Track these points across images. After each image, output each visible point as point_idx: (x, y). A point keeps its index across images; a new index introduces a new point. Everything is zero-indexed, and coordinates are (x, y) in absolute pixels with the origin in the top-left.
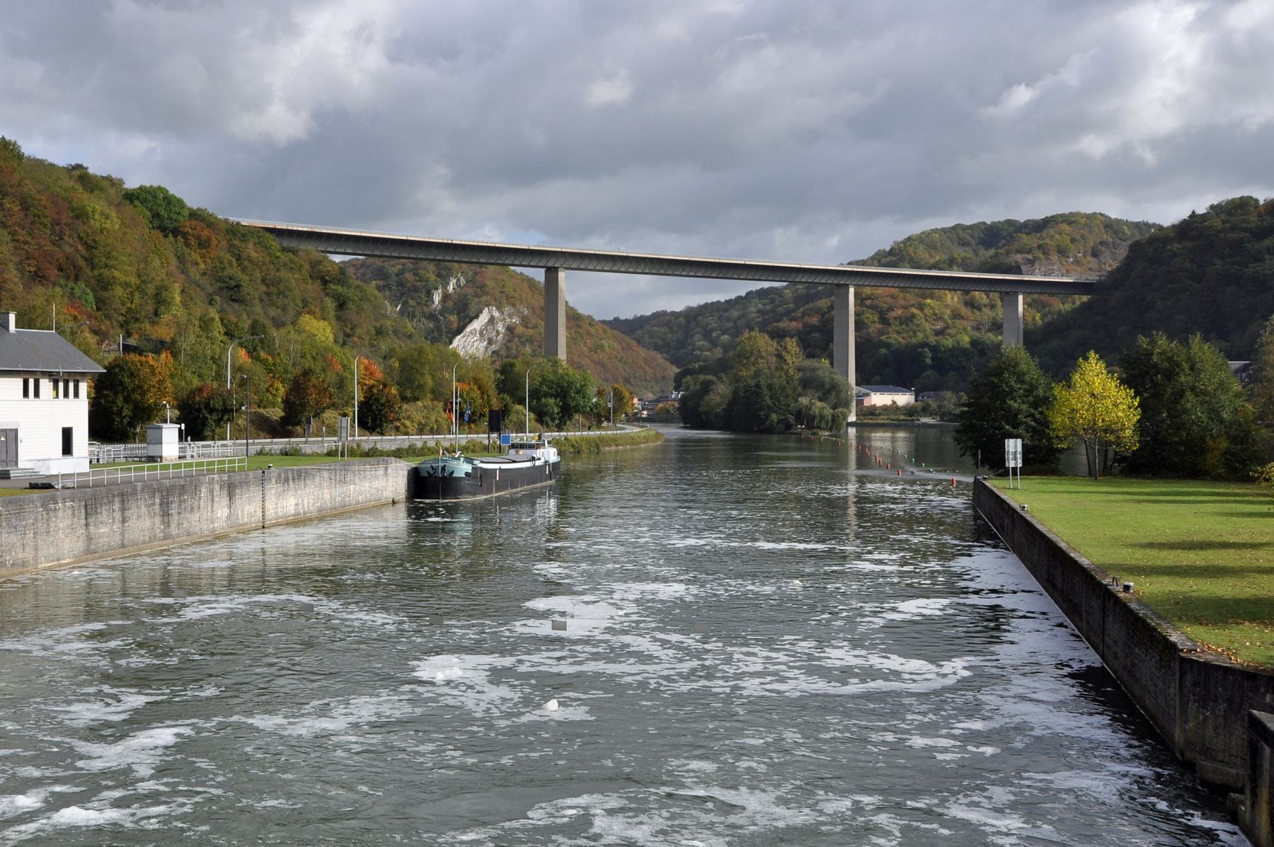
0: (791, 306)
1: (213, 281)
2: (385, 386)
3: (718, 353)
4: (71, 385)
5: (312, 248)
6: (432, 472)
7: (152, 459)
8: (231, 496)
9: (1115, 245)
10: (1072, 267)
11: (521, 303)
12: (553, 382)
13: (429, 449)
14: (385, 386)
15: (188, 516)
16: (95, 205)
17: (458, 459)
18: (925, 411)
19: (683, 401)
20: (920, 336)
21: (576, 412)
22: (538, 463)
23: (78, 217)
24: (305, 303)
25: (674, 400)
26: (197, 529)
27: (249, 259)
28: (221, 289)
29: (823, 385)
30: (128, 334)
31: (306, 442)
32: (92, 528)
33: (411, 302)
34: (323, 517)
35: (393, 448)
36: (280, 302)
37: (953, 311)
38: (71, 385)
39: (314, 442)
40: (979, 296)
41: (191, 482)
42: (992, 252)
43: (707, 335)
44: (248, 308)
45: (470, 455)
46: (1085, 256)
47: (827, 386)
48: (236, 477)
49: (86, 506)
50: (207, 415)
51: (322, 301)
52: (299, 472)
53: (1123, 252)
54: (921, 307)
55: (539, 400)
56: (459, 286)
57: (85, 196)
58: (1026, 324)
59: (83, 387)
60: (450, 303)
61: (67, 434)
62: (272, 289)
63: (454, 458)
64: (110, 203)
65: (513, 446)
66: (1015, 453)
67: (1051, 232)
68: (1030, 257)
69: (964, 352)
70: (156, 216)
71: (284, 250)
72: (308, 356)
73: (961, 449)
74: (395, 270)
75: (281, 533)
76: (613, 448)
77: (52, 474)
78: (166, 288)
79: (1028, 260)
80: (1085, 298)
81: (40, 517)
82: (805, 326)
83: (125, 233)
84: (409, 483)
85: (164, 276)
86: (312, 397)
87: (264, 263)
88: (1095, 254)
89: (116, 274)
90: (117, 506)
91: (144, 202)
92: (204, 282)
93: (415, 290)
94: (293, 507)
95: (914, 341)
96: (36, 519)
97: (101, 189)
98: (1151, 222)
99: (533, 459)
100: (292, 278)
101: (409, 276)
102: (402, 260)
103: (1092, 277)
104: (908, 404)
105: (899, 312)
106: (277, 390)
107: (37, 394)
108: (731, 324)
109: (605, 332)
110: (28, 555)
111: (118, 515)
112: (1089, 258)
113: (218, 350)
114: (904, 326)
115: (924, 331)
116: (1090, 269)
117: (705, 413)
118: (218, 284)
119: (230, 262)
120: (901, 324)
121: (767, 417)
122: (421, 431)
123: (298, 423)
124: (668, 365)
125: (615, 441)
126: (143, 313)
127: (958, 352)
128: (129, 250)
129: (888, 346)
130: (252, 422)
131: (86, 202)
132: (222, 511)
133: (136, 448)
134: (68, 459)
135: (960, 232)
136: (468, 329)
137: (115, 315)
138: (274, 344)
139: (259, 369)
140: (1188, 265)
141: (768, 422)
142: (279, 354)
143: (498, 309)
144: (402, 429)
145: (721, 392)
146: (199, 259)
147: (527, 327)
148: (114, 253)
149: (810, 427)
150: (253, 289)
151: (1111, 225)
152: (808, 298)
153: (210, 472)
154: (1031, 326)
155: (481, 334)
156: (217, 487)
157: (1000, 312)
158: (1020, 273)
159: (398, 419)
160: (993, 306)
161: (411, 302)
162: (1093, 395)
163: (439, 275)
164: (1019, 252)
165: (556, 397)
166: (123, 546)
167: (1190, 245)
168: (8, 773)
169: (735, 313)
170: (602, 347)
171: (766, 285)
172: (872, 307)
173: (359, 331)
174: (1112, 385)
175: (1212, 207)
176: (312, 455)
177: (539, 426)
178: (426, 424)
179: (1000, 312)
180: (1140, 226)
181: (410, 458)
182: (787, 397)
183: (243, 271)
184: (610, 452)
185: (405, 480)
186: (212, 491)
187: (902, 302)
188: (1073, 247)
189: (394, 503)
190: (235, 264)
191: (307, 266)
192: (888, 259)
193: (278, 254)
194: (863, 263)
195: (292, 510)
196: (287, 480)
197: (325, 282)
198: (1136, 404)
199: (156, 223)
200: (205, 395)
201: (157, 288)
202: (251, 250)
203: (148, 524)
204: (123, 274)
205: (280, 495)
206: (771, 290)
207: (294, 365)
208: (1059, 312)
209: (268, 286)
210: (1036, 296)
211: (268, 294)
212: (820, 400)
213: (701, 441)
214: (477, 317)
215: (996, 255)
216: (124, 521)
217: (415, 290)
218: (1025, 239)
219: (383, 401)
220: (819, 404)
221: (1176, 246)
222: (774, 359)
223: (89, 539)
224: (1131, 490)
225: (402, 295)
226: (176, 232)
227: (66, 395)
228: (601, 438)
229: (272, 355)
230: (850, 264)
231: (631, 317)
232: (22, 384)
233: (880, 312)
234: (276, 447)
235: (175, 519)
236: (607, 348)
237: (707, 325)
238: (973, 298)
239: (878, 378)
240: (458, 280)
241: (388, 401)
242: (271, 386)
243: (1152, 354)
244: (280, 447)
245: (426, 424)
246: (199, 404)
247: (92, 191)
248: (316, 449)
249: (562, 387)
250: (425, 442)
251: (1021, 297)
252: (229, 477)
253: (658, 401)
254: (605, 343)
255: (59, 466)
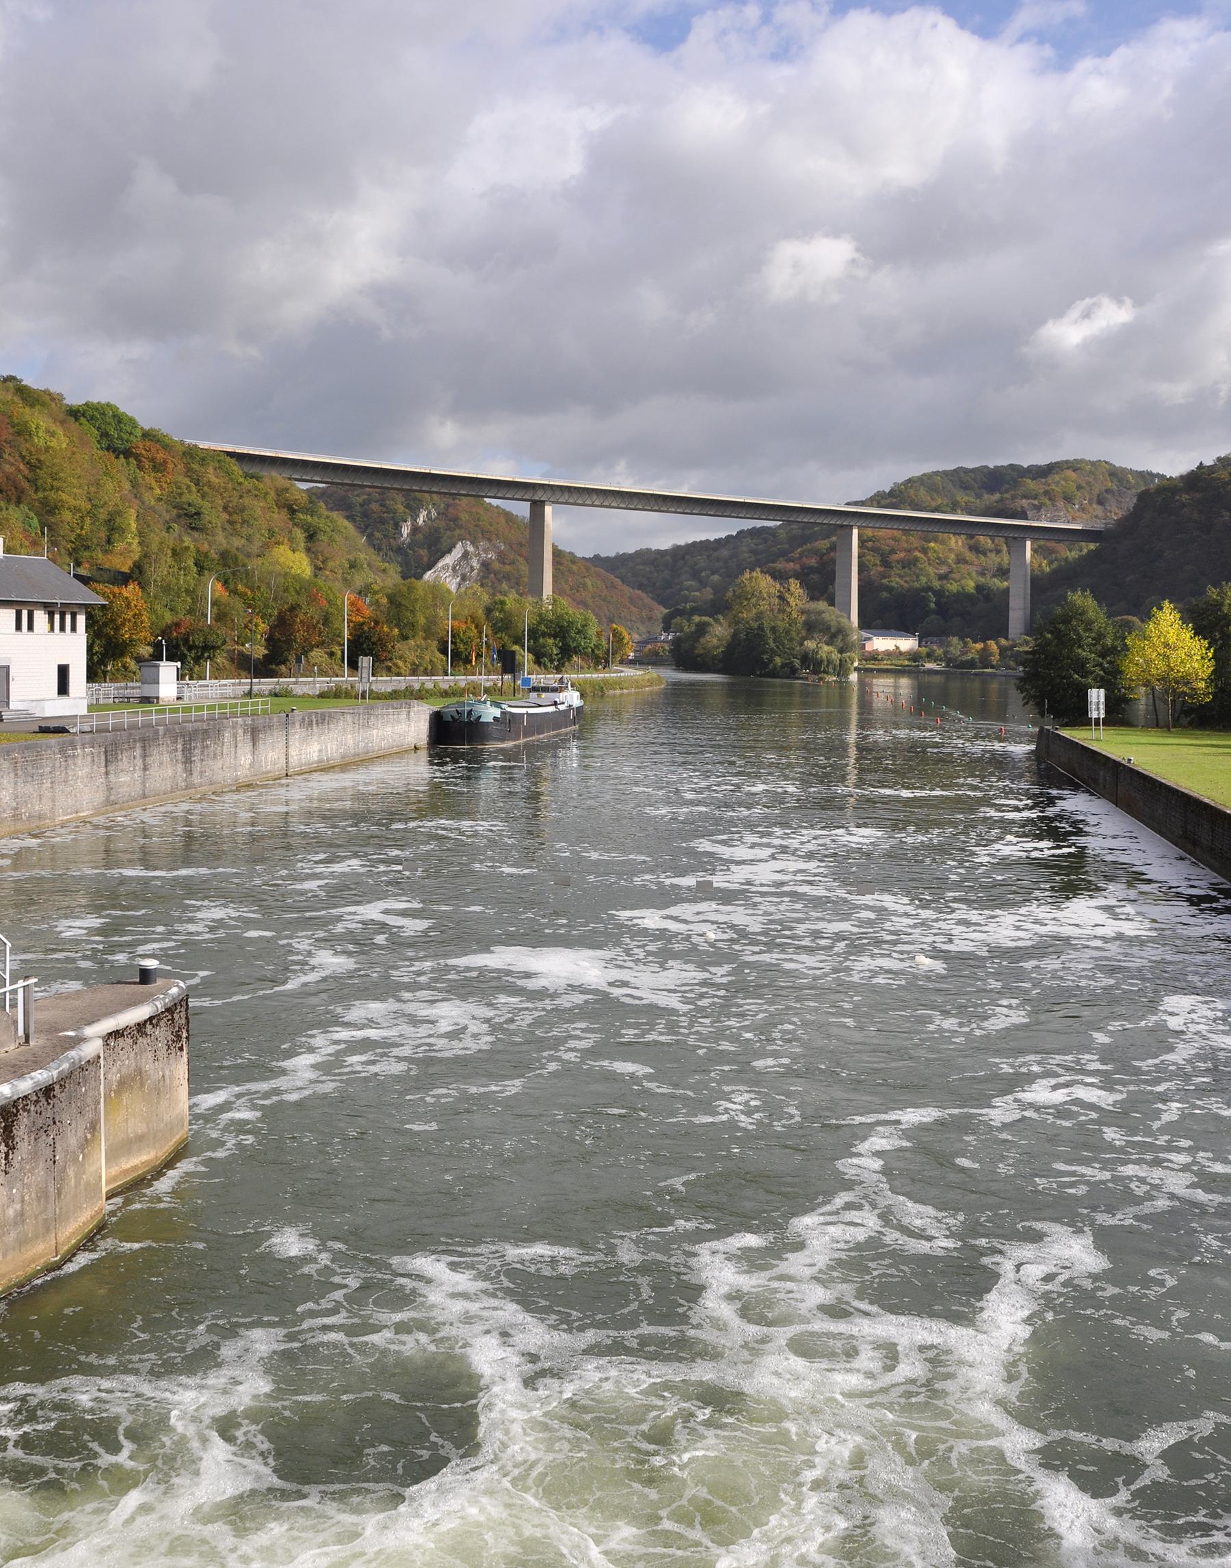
0: (786, 546)
1: (170, 508)
2: (377, 623)
3: (708, 594)
4: (68, 618)
5: (278, 478)
6: (457, 716)
7: (146, 700)
8: (254, 741)
9: (1120, 494)
10: (1078, 514)
11: (498, 537)
12: (551, 621)
13: (427, 691)
14: (377, 623)
15: (211, 763)
16: (39, 421)
17: (485, 702)
18: (930, 656)
19: (676, 643)
20: (924, 580)
21: (576, 653)
22: (561, 707)
23: (19, 434)
24: (271, 533)
25: (664, 641)
26: (219, 778)
27: (209, 484)
28: (179, 516)
29: (829, 628)
30: (78, 564)
31: (296, 683)
32: (112, 777)
33: (378, 535)
34: (345, 765)
35: (389, 690)
36: (245, 531)
37: (957, 556)
38: (68, 618)
39: (305, 683)
40: (984, 541)
41: (214, 725)
42: (997, 496)
43: (695, 575)
44: (210, 538)
45: (497, 698)
46: (1090, 503)
47: (833, 630)
48: (260, 721)
49: (106, 752)
50: (185, 652)
51: (290, 532)
52: (323, 715)
53: (1130, 502)
54: (924, 551)
55: (536, 640)
56: (430, 519)
57: (27, 410)
58: (1032, 570)
59: (81, 620)
60: (420, 536)
61: (63, 672)
62: (236, 517)
63: (480, 701)
64: (55, 420)
65: (535, 689)
66: (1098, 703)
67: (1057, 478)
68: (1036, 502)
69: (969, 597)
70: (105, 435)
71: (246, 476)
72: (291, 590)
73: (1024, 698)
74: (360, 500)
75: (320, 778)
76: (618, 692)
77: (47, 715)
78: (119, 513)
79: (1034, 505)
80: (1092, 546)
81: (57, 765)
82: (803, 567)
83: (74, 453)
84: (431, 728)
85: (118, 501)
86: (300, 635)
87: (226, 490)
88: (1101, 502)
89: (64, 497)
90: (138, 752)
91: (92, 419)
92: (161, 507)
93: (382, 521)
94: (316, 754)
95: (916, 585)
96: (54, 766)
97: (43, 404)
98: (1154, 471)
99: (555, 704)
100: (257, 507)
101: (375, 507)
102: (367, 490)
103: (1098, 525)
104: (911, 650)
105: (902, 555)
106: (256, 626)
107: (31, 628)
108: (721, 564)
109: (588, 570)
110: (45, 806)
111: (139, 762)
112: (1095, 506)
113: (192, 583)
114: (906, 570)
115: (928, 575)
116: (1096, 517)
117: (700, 655)
118: (175, 511)
119: (188, 487)
120: (904, 567)
121: (771, 660)
122: (414, 672)
123: (284, 662)
124: (655, 605)
125: (619, 684)
126: (95, 541)
127: (962, 597)
128: (78, 471)
129: (889, 589)
130: (232, 660)
131: (27, 418)
132: (245, 758)
133: (135, 689)
134: (64, 700)
135: (962, 475)
136: (440, 564)
137: (64, 543)
138: (253, 576)
139: (238, 603)
140: (1196, 516)
141: (771, 666)
142: (259, 588)
143: (473, 543)
144: (394, 669)
145: (719, 633)
146: (154, 483)
147: (504, 563)
148: (62, 475)
149: (816, 672)
150: (214, 516)
151: (1116, 474)
152: (804, 539)
153: (234, 715)
154: (1037, 572)
155: (454, 569)
156: (240, 731)
157: (1006, 558)
158: (1026, 518)
159: (391, 659)
160: (998, 552)
161: (378, 535)
162: (1167, 645)
163: (408, 506)
164: (1024, 497)
165: (555, 637)
166: (144, 796)
167: (1198, 495)
168: (324, 1051)
169: (725, 553)
170: (585, 586)
171: (759, 524)
172: (873, 549)
173: (331, 564)
174: (1187, 635)
175: (1219, 459)
176: (303, 696)
177: (536, 667)
178: (420, 664)
179: (1006, 558)
180: (1146, 476)
181: (431, 700)
182: (791, 640)
183: (203, 497)
184: (614, 696)
185: (427, 725)
186: (235, 736)
187: (905, 545)
188: (1079, 494)
189: (416, 748)
190: (194, 489)
191: (272, 493)
192: (888, 501)
193: (241, 480)
194: (862, 504)
195: (315, 757)
196: (310, 724)
197: (292, 512)
198: (1210, 655)
199: (105, 443)
200: (183, 630)
201: (109, 513)
202: (211, 475)
203: (170, 772)
204: (72, 496)
205: (304, 740)
206: (764, 529)
207: (275, 599)
208: (1066, 559)
209: (230, 515)
210: (1042, 543)
211: (231, 523)
212: (828, 644)
213: (692, 684)
214: (449, 551)
215: (1002, 500)
216: (145, 769)
217: (382, 521)
218: (1030, 484)
219: (374, 639)
220: (826, 648)
221: (1185, 497)
222: (777, 601)
223: (110, 789)
224: (1214, 742)
225: (367, 527)
226: (127, 453)
227: (62, 629)
228: (605, 681)
229: (252, 589)
230: (848, 504)
231: (612, 554)
232: (14, 615)
233: (882, 555)
234: (264, 687)
235: (197, 767)
236: (590, 586)
237: (696, 564)
238: (978, 541)
239: (879, 622)
240: (429, 512)
241: (380, 639)
242: (250, 622)
243: (1222, 604)
244: (269, 687)
245: (420, 664)
246: (177, 639)
247: (32, 406)
248: (306, 690)
249: (561, 627)
250: (423, 684)
251: (1028, 543)
252: (253, 720)
253: (646, 642)
254: (589, 582)
255: (56, 708)
